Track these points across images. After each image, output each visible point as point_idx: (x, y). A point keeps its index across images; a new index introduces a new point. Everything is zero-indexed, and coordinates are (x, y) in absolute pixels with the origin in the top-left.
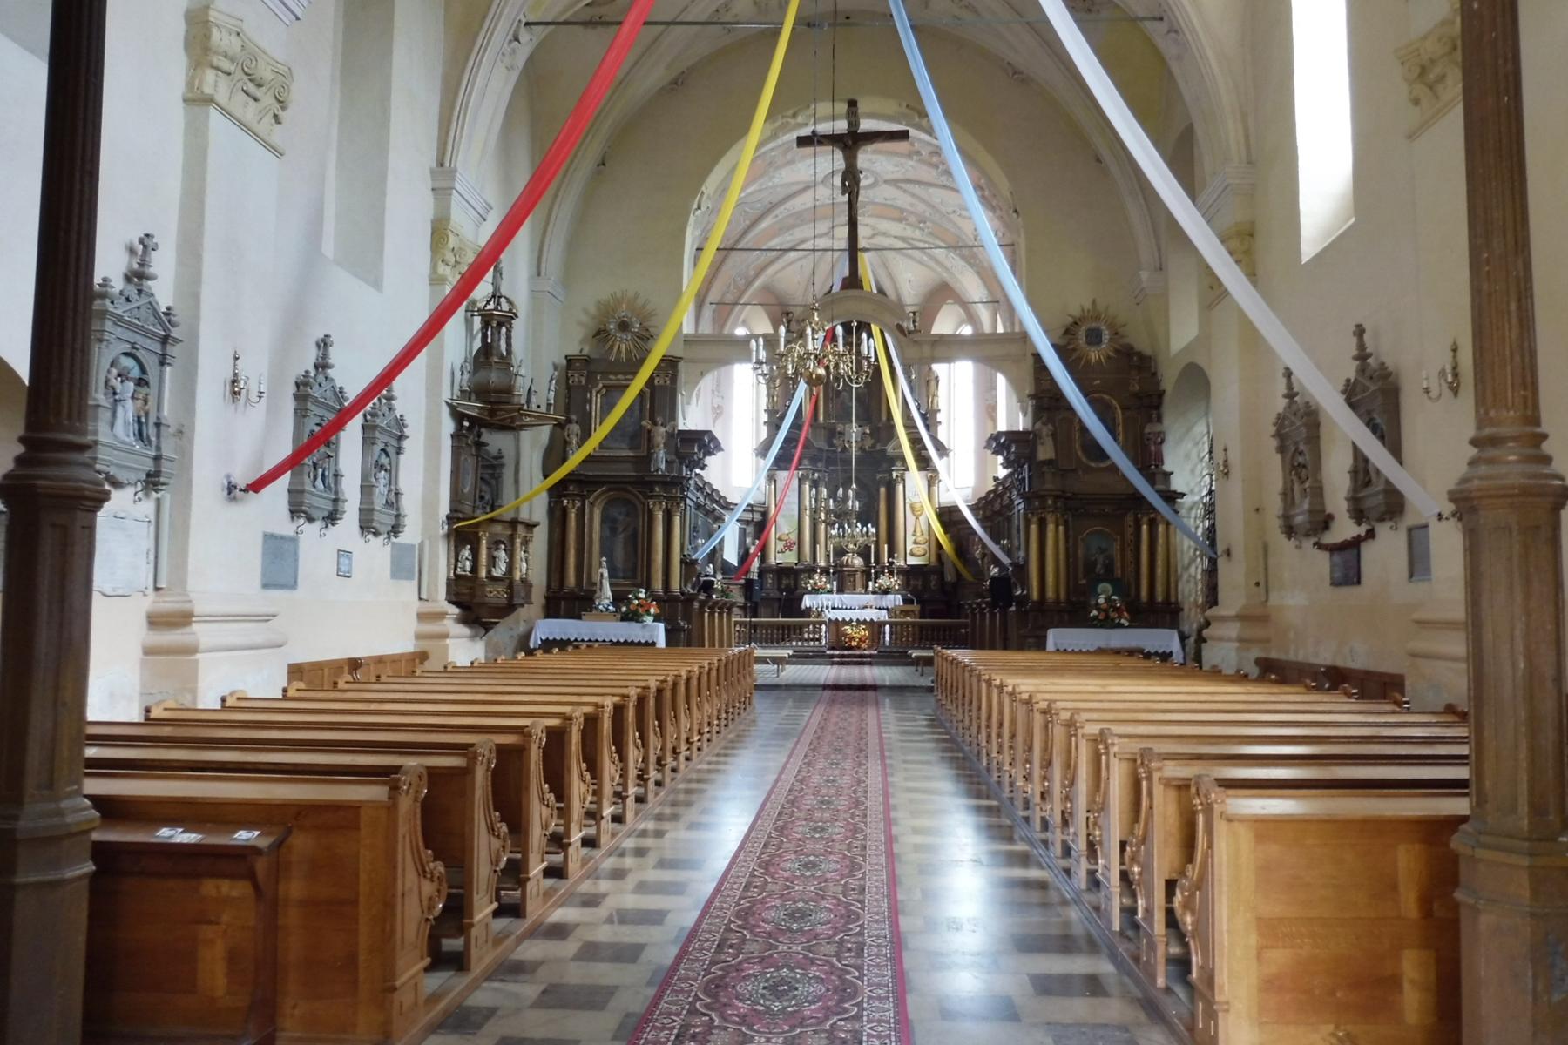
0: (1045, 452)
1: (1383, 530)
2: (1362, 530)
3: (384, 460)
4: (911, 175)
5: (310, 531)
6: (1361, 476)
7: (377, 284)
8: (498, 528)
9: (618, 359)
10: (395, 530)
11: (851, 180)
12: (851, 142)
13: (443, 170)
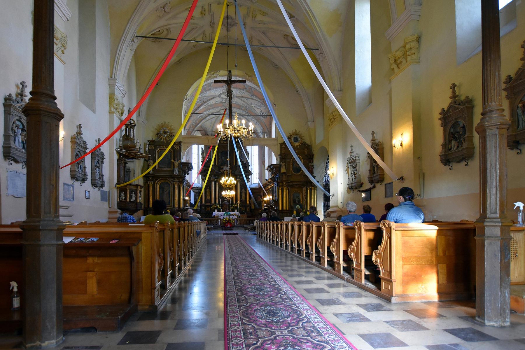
0: (283, 170)
1: (378, 185)
2: (371, 186)
3: (98, 165)
4: (243, 95)
5: (77, 184)
6: (372, 171)
7: (94, 111)
8: (132, 187)
9: (163, 142)
10: (102, 186)
11: (229, 94)
12: (229, 82)
13: (112, 78)
